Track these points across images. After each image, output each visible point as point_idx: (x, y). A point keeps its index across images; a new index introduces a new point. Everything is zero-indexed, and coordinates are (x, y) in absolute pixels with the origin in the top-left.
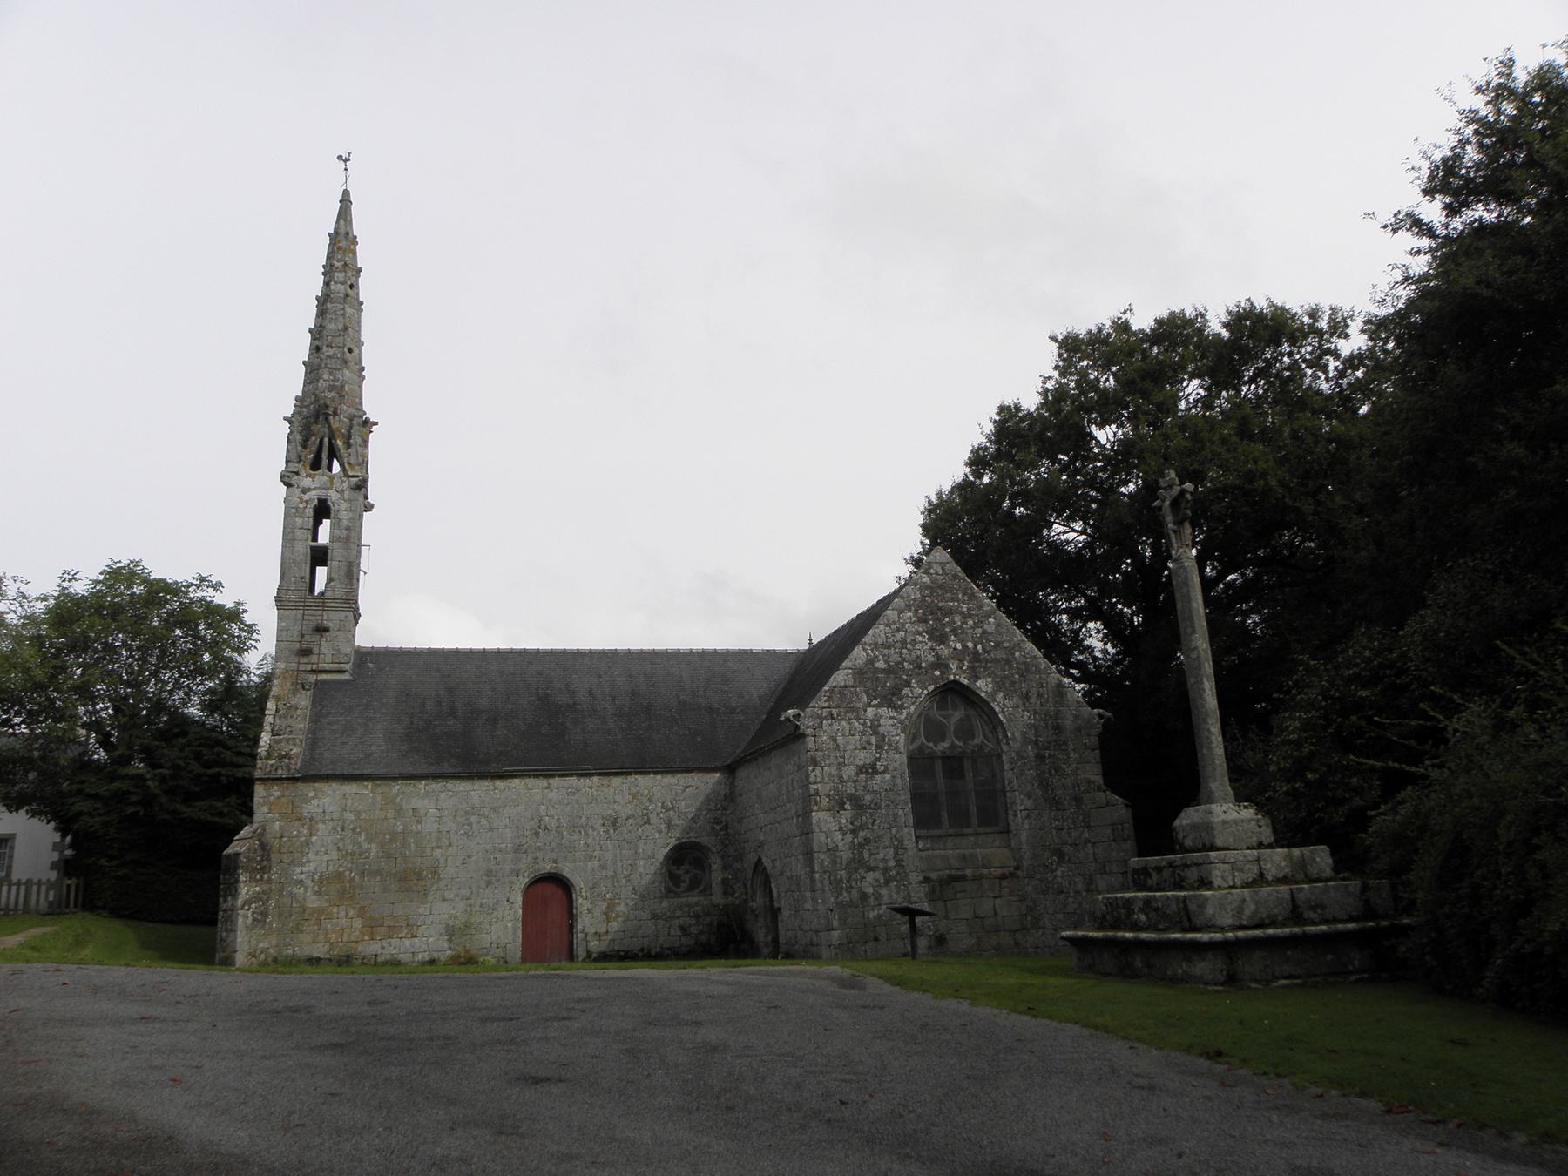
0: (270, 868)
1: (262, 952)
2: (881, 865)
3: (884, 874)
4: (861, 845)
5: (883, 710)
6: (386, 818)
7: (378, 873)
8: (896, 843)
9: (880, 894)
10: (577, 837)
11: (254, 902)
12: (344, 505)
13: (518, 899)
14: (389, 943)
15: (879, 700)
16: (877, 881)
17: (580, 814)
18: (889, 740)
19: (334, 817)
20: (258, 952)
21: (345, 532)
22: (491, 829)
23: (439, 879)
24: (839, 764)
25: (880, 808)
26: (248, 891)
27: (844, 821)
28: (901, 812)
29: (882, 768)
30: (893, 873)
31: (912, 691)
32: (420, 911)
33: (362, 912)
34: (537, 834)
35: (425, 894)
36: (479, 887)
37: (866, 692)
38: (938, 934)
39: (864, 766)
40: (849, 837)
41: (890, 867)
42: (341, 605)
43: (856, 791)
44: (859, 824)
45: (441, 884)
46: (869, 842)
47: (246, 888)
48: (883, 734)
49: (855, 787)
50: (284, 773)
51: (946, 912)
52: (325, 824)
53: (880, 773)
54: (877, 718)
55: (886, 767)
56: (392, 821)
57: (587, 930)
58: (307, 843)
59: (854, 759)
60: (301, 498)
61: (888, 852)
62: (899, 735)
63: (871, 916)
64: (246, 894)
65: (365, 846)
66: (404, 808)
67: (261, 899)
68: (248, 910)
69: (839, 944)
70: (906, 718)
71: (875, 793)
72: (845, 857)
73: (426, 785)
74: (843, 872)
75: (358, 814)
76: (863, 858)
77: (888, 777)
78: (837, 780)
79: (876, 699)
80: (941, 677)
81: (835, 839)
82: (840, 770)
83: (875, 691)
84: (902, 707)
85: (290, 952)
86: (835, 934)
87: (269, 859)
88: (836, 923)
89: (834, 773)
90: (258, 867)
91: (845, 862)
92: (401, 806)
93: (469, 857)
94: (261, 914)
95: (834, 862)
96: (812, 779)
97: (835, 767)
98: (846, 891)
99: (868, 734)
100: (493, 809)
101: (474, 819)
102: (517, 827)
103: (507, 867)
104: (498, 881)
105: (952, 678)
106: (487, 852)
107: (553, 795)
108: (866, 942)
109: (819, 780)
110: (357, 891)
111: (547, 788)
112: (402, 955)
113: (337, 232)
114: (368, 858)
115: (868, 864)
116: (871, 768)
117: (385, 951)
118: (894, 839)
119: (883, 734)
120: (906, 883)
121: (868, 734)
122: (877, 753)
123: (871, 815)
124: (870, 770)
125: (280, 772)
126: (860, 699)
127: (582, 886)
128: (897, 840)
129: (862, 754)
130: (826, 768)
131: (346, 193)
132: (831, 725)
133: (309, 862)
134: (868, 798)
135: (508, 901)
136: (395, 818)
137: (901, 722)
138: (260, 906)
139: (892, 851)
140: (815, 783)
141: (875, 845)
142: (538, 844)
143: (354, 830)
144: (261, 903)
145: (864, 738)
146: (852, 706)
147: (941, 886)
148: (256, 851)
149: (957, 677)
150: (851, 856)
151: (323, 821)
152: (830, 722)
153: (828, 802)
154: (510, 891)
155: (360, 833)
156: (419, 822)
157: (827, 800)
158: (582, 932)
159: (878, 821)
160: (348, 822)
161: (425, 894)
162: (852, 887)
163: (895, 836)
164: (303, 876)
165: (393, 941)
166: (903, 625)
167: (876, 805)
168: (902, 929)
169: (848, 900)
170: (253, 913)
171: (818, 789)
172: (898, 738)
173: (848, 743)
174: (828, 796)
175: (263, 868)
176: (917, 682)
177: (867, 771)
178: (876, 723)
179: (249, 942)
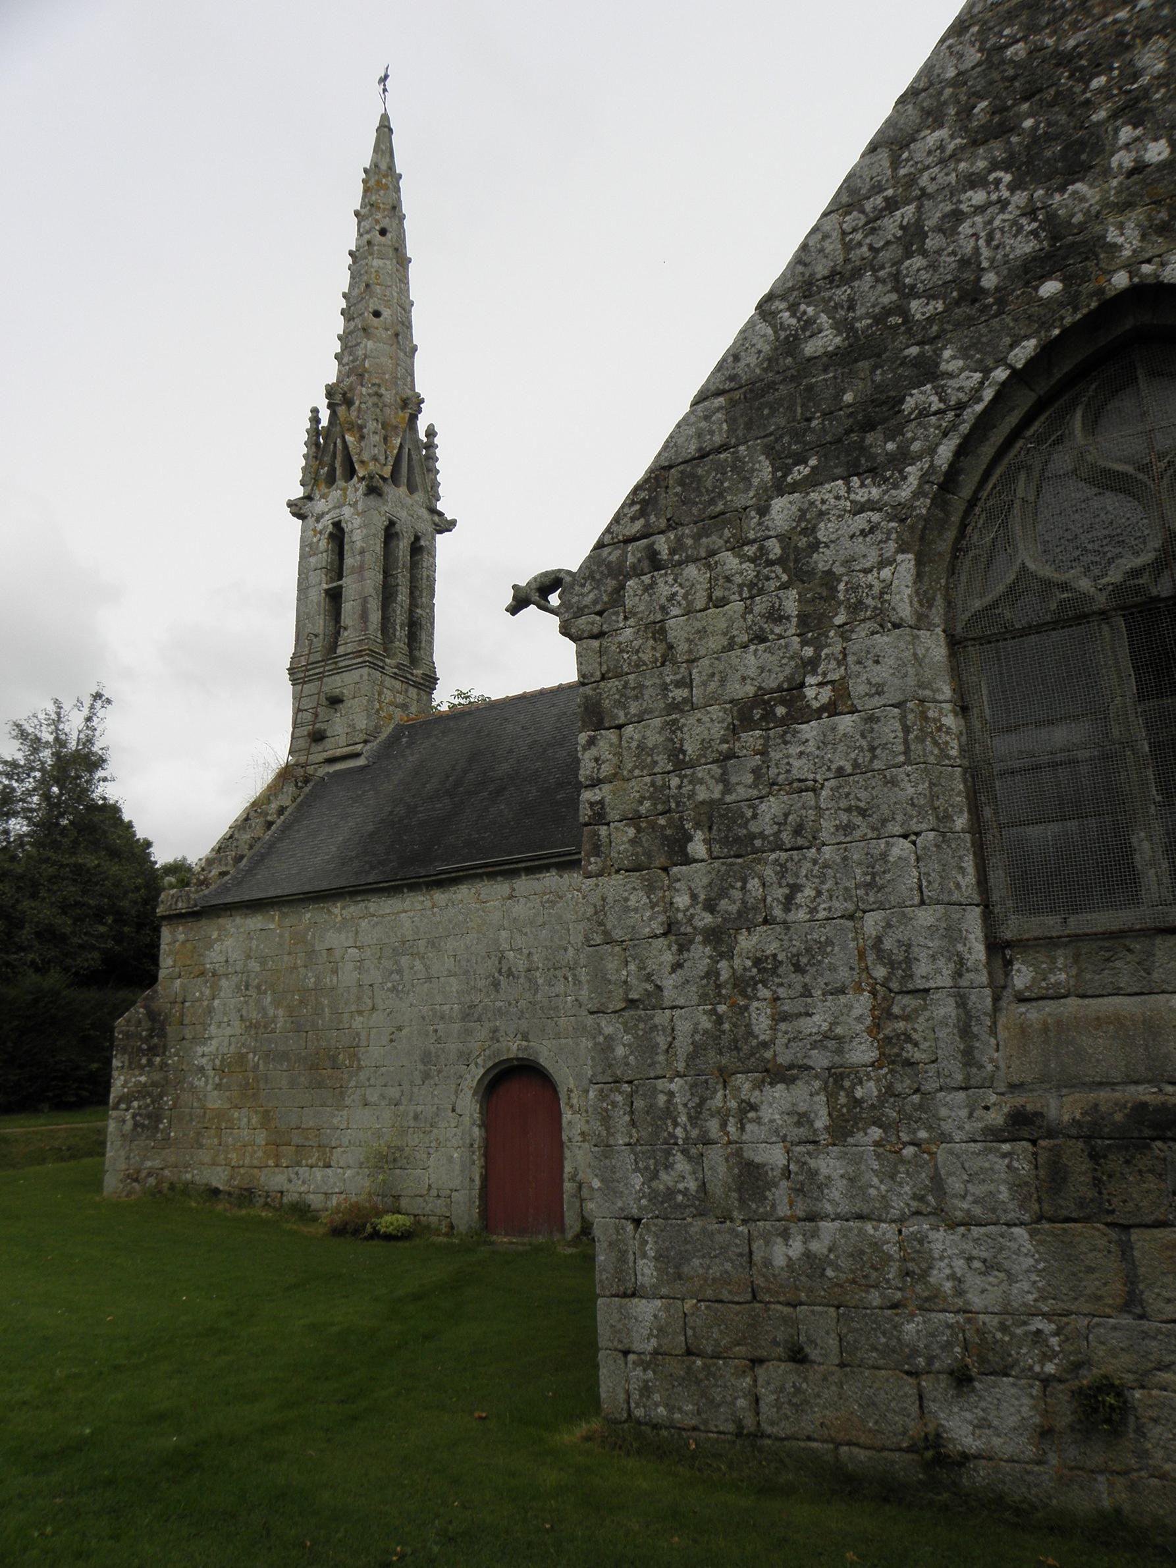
0: (165, 1047)
1: (149, 1175)
2: (820, 1060)
3: (831, 1097)
4: (743, 985)
5: (830, 493)
6: (295, 968)
7: (284, 1056)
8: (880, 972)
9: (813, 1174)
10: (560, 988)
11: (136, 1099)
12: (357, 521)
13: (469, 1105)
14: (297, 1173)
15: (813, 462)
16: (803, 1119)
17: (564, 943)
18: (853, 588)
19: (238, 969)
20: (144, 1174)
21: (358, 557)
22: (429, 979)
23: (360, 1068)
24: (674, 707)
25: (815, 841)
26: (126, 1082)
27: (682, 901)
28: (902, 847)
29: (826, 694)
30: (868, 1090)
31: (941, 393)
32: (335, 1121)
33: (266, 1117)
34: (496, 985)
35: (341, 1093)
36: (412, 1083)
37: (769, 451)
38: (1087, 1378)
39: (759, 699)
40: (700, 955)
41: (855, 1069)
42: (354, 661)
43: (727, 790)
44: (733, 908)
45: (363, 1076)
46: (774, 972)
47: (122, 1078)
48: (830, 572)
49: (724, 780)
50: (185, 905)
51: (1131, 1280)
52: (227, 979)
53: (818, 714)
54: (807, 523)
55: (841, 689)
56: (302, 970)
57: (581, 1176)
58: (210, 1010)
59: (723, 681)
60: (314, 530)
61: (850, 1007)
62: (890, 562)
63: (780, 1261)
64: (123, 1086)
65: (271, 1012)
66: (317, 948)
67: (150, 1094)
68: (127, 1110)
69: (656, 1353)
70: (917, 495)
71: (802, 787)
72: (683, 1028)
73: (343, 908)
74: (676, 1085)
75: (263, 961)
76: (750, 1034)
77: (846, 723)
78: (663, 763)
79: (805, 462)
80: (1070, 298)
81: (651, 965)
82: (674, 726)
83: (797, 436)
84: (902, 458)
85: (189, 1176)
86: (646, 1310)
87: (163, 1035)
88: (647, 1271)
89: (654, 738)
90: (145, 1047)
91: (683, 1046)
92: (313, 946)
93: (400, 1029)
94: (149, 1116)
95: (645, 1047)
96: (586, 771)
97: (657, 722)
98: (684, 1152)
99: (772, 585)
100: (432, 943)
101: (405, 961)
102: (466, 972)
103: (453, 1047)
104: (439, 1072)
105: (1121, 280)
106: (423, 1018)
107: (520, 910)
108: (756, 1362)
109: (606, 770)
110: (262, 1086)
111: (511, 897)
112: (311, 1196)
113: (375, 165)
114: (273, 1031)
115: (768, 1055)
116: (783, 702)
117: (291, 1187)
118: (871, 957)
119: (830, 572)
120: (923, 1134)
121: (772, 585)
122: (804, 643)
123: (782, 870)
124: (781, 711)
125: (180, 905)
126: (747, 480)
127: (572, 1086)
128: (882, 956)
129: (751, 660)
130: (629, 729)
131: (385, 118)
132: (649, 588)
133: (210, 1038)
134: (771, 808)
135: (453, 1110)
136: (306, 967)
137: (900, 513)
138: (148, 1106)
139: (862, 1004)
140: (596, 783)
141: (796, 979)
142: (498, 1004)
143: (258, 987)
144: (149, 1101)
145: (761, 605)
146: (720, 507)
147: (1094, 1156)
148: (139, 1022)
149: (1146, 268)
150: (706, 1023)
151: (226, 975)
152: (646, 579)
153: (633, 842)
154: (456, 1092)
155: (265, 993)
156: (335, 971)
157: (631, 832)
158: (573, 1179)
159: (809, 892)
160: (253, 975)
161: (341, 1093)
162: (708, 1142)
163: (879, 940)
164: (204, 1061)
165: (302, 1170)
166: (912, 180)
167: (798, 831)
168: (910, 1327)
169: (692, 1186)
170: (134, 1116)
171: (601, 802)
172: (886, 573)
173: (703, 632)
174: (634, 819)
175: (150, 1049)
176: (964, 352)
177: (769, 715)
178: (803, 542)
179: (128, 1158)
